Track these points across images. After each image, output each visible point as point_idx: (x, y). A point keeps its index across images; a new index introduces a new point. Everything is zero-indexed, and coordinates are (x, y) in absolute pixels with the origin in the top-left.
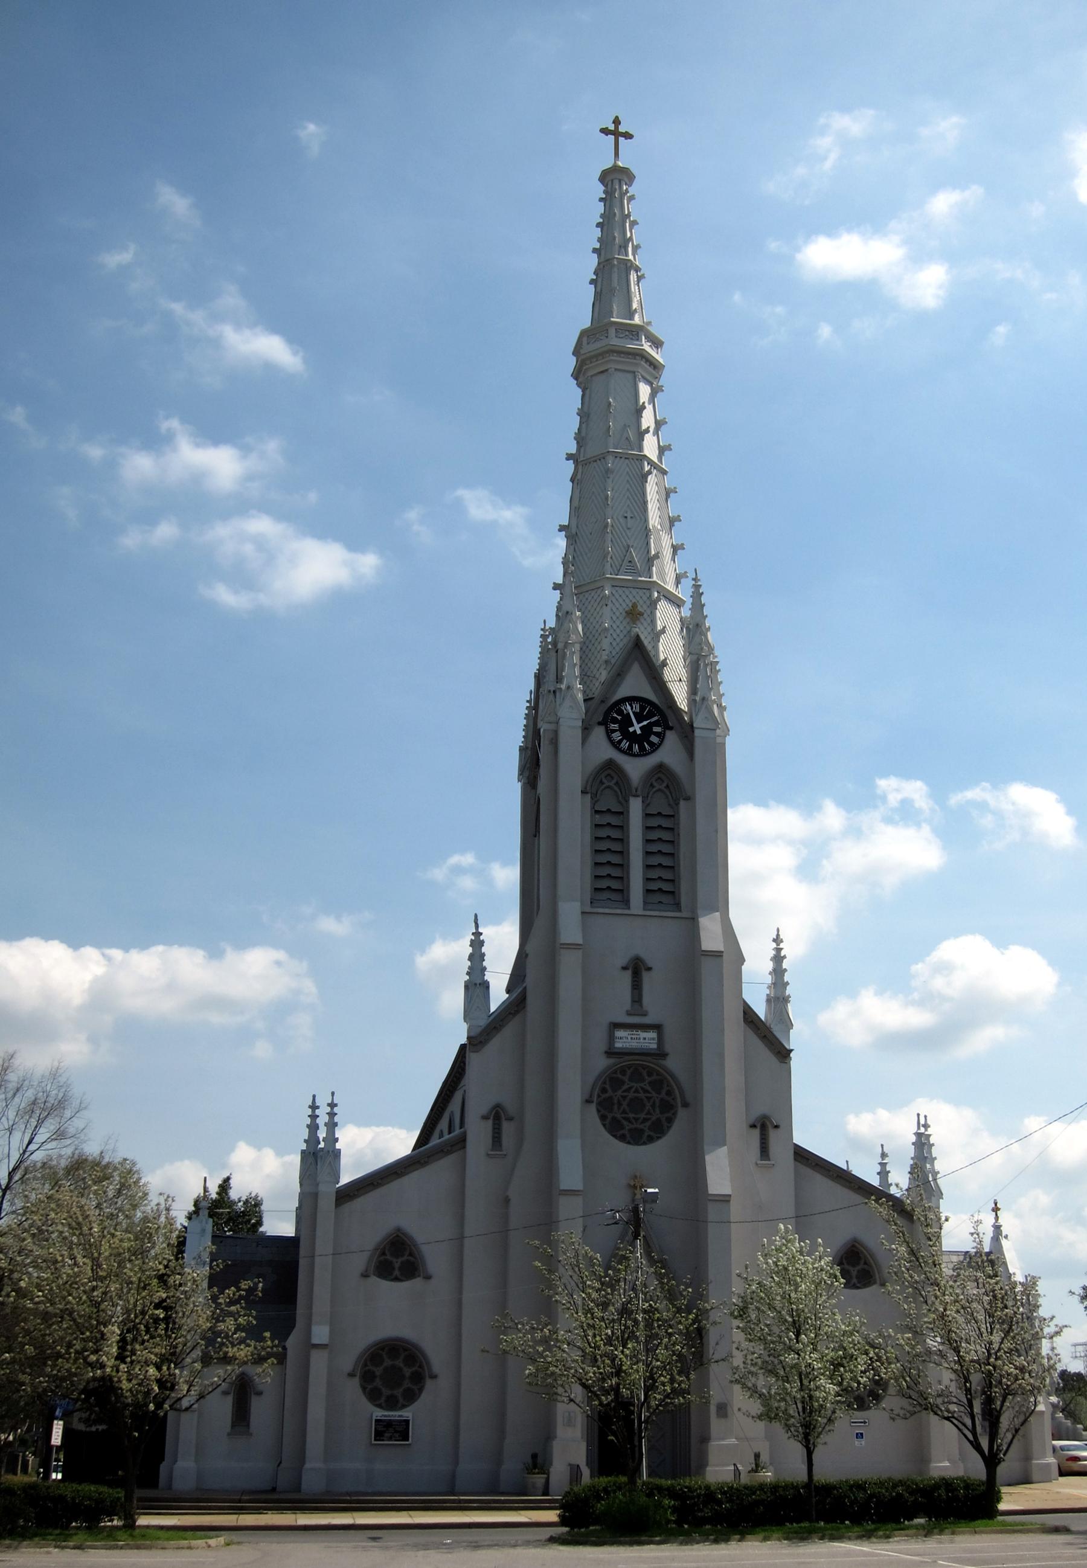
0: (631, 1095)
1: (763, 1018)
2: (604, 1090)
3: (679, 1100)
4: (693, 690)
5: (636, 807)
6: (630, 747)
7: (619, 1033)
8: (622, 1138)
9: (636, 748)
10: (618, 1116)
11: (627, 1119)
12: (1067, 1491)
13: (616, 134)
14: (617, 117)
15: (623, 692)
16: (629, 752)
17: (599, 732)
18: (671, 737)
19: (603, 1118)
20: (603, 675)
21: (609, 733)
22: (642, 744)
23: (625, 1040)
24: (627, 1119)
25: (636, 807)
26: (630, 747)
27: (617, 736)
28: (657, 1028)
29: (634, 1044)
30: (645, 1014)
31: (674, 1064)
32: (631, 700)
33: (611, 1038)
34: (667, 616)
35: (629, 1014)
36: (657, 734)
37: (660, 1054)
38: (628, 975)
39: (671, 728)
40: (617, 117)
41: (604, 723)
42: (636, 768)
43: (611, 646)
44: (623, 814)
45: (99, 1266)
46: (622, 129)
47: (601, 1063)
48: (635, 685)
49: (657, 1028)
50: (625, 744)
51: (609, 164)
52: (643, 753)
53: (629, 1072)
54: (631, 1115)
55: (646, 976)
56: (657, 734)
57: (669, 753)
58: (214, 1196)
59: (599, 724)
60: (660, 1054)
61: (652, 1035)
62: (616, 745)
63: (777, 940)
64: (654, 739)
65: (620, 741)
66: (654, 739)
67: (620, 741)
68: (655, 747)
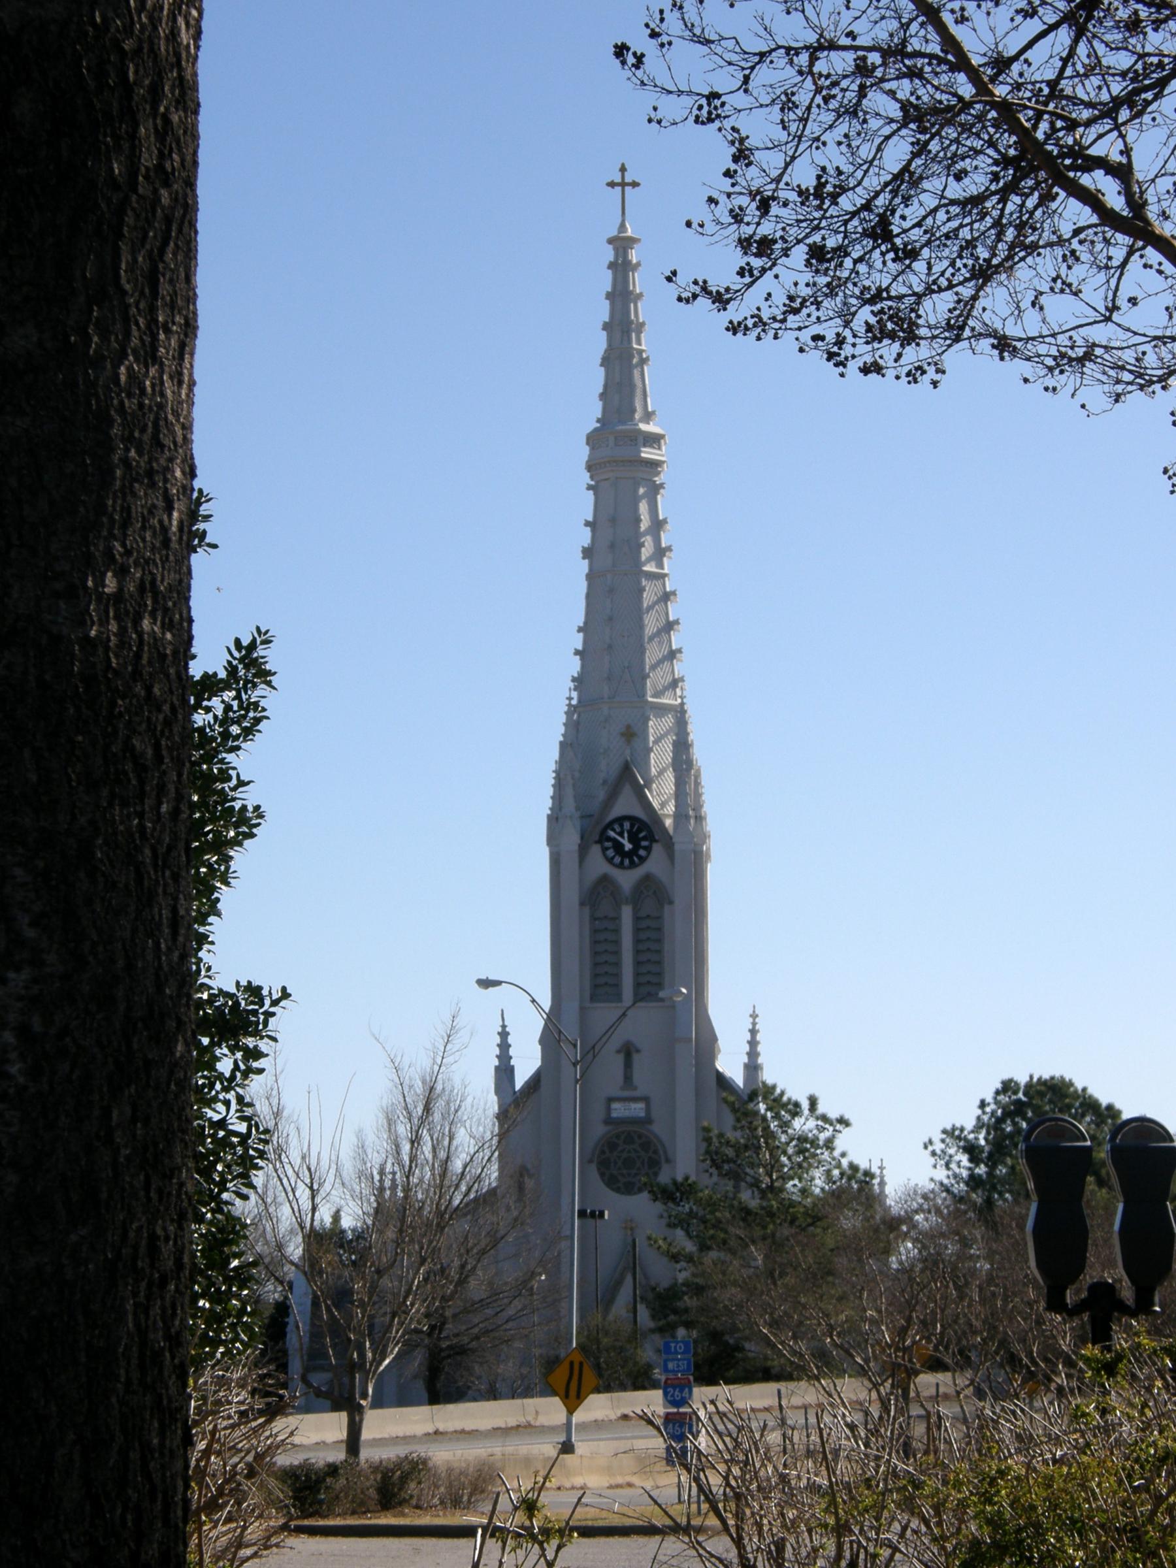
0: (625, 1155)
1: (741, 1085)
2: (603, 1152)
3: (663, 1158)
4: (680, 794)
5: (627, 913)
6: (622, 862)
7: (615, 1105)
8: (618, 1190)
9: (627, 862)
10: (615, 1172)
11: (623, 1175)
12: (381, 1368)
13: (623, 184)
14: (623, 165)
15: (618, 810)
16: (621, 866)
17: (596, 850)
18: (657, 849)
19: (602, 1175)
20: (601, 795)
21: (604, 850)
22: (631, 859)
23: (619, 1110)
24: (623, 1175)
25: (627, 913)
26: (622, 862)
27: (611, 853)
28: (646, 1099)
29: (627, 1114)
30: (635, 1089)
31: (658, 1128)
32: (620, 820)
33: (609, 1109)
34: (657, 727)
35: (622, 1089)
36: (645, 848)
37: (648, 1120)
38: (620, 1058)
39: (656, 841)
40: (623, 165)
41: (599, 842)
42: (626, 879)
43: (608, 768)
44: (617, 919)
45: (955, 155)
46: (628, 180)
47: (600, 1130)
48: (624, 806)
49: (646, 1099)
50: (617, 860)
51: (614, 233)
52: (633, 865)
53: (623, 1137)
54: (625, 1172)
55: (636, 1057)
56: (645, 848)
57: (655, 863)
58: (328, 1225)
59: (596, 842)
60: (648, 1120)
61: (641, 1105)
62: (610, 861)
63: (754, 1016)
64: (642, 852)
65: (613, 858)
66: (642, 852)
67: (613, 858)
68: (642, 860)
